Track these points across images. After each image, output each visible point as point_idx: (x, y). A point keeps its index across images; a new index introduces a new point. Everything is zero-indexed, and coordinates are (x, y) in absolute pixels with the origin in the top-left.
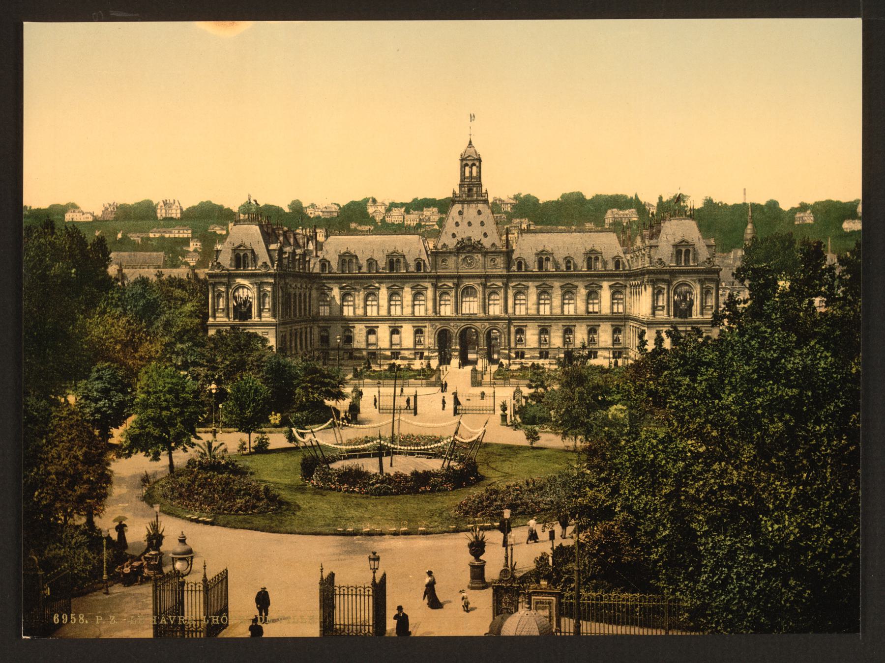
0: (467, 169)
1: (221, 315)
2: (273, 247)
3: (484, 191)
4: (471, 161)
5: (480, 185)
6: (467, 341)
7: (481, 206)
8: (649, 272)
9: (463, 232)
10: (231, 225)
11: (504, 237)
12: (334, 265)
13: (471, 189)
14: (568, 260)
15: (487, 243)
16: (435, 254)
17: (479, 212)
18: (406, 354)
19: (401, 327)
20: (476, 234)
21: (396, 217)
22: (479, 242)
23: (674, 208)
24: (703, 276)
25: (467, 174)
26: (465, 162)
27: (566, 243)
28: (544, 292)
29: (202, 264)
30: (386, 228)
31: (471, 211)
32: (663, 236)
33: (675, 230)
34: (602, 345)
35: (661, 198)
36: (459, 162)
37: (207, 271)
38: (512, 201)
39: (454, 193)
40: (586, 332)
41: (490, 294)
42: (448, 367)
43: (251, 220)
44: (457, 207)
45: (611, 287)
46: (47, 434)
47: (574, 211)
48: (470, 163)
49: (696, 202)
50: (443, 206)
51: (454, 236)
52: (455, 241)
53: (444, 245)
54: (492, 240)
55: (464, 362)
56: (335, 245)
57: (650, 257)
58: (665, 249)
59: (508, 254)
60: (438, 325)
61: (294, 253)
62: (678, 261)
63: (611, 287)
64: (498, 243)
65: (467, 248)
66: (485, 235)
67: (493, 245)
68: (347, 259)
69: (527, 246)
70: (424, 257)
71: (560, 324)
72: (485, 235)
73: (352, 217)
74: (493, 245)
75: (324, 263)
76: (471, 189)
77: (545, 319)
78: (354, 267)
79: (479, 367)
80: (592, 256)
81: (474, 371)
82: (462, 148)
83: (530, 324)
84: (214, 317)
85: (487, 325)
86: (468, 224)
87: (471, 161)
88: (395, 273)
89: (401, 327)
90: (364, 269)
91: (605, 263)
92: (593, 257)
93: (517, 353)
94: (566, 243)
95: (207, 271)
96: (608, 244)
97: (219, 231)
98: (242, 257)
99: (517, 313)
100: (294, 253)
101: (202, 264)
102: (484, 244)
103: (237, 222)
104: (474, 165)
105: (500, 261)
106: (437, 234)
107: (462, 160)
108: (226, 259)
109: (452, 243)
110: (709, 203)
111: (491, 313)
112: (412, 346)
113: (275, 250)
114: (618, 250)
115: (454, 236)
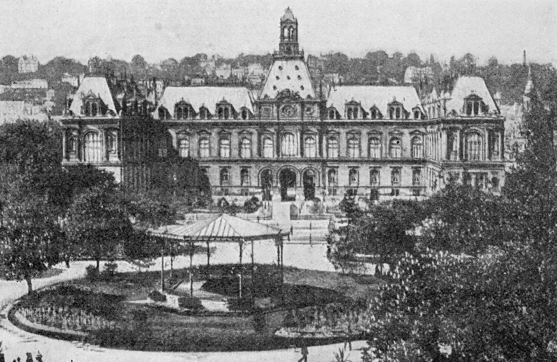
0: (286, 31)
1: (74, 156)
2: (120, 96)
3: (300, 50)
4: (289, 25)
5: (296, 45)
6: (288, 179)
7: (298, 63)
8: (444, 122)
9: (282, 86)
10: (82, 77)
11: (318, 89)
12: (172, 112)
13: (289, 49)
14: (374, 110)
15: (303, 95)
16: (258, 104)
17: (297, 68)
18: (235, 191)
19: (208, 167)
20: (293, 86)
21: (224, 73)
22: (296, 94)
23: (466, 67)
24: (106, 126)
25: (286, 34)
26: (284, 25)
27: (376, 97)
28: (354, 136)
29: (56, 111)
30: (211, 82)
31: (289, 66)
32: (455, 91)
33: (467, 86)
34: (403, 184)
35: (453, 58)
36: (279, 25)
37: (62, 117)
38: (325, 59)
39: (275, 52)
40: (369, 173)
41: (306, 139)
42: (270, 202)
43: (97, 74)
44: (278, 63)
45: (411, 133)
46: (401, 259)
47: (376, 69)
48: (289, 26)
49: (481, 62)
50: (267, 61)
51: (275, 88)
52: (275, 92)
53: (266, 96)
54: (307, 91)
55: (285, 198)
56: (170, 97)
57: (445, 109)
58: (456, 102)
59: (322, 105)
60: (262, 166)
61: (136, 103)
62: (469, 113)
63: (369, 134)
64: (313, 95)
65: (287, 98)
66: (302, 88)
67: (309, 96)
68: (353, 107)
69: (339, 97)
70: (250, 107)
71: (389, 165)
72: (302, 88)
73: (189, 71)
74: (309, 96)
75: (163, 111)
76: (289, 49)
77: (375, 161)
78: (359, 113)
79: (297, 204)
80: (223, 108)
81: (293, 207)
82: (281, 14)
83: (342, 165)
84: (68, 158)
85: (304, 166)
86: (289, 78)
87: (289, 25)
88: (226, 121)
89: (338, 167)
90: (412, 116)
91: (365, 114)
92: (395, 107)
93: (330, 191)
94: (376, 97)
95: (62, 117)
96: (409, 98)
97: (74, 82)
98: (93, 105)
99: (331, 156)
100: (136, 103)
101: (56, 111)
102: (301, 96)
103: (87, 75)
104: (291, 27)
105: (316, 109)
106: (260, 87)
107: (282, 23)
108: (77, 107)
109: (273, 95)
110: (493, 63)
111: (308, 155)
112: (389, 184)
113: (120, 99)
114: (417, 102)
115: (275, 88)
